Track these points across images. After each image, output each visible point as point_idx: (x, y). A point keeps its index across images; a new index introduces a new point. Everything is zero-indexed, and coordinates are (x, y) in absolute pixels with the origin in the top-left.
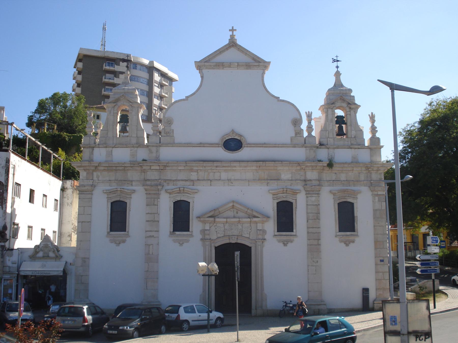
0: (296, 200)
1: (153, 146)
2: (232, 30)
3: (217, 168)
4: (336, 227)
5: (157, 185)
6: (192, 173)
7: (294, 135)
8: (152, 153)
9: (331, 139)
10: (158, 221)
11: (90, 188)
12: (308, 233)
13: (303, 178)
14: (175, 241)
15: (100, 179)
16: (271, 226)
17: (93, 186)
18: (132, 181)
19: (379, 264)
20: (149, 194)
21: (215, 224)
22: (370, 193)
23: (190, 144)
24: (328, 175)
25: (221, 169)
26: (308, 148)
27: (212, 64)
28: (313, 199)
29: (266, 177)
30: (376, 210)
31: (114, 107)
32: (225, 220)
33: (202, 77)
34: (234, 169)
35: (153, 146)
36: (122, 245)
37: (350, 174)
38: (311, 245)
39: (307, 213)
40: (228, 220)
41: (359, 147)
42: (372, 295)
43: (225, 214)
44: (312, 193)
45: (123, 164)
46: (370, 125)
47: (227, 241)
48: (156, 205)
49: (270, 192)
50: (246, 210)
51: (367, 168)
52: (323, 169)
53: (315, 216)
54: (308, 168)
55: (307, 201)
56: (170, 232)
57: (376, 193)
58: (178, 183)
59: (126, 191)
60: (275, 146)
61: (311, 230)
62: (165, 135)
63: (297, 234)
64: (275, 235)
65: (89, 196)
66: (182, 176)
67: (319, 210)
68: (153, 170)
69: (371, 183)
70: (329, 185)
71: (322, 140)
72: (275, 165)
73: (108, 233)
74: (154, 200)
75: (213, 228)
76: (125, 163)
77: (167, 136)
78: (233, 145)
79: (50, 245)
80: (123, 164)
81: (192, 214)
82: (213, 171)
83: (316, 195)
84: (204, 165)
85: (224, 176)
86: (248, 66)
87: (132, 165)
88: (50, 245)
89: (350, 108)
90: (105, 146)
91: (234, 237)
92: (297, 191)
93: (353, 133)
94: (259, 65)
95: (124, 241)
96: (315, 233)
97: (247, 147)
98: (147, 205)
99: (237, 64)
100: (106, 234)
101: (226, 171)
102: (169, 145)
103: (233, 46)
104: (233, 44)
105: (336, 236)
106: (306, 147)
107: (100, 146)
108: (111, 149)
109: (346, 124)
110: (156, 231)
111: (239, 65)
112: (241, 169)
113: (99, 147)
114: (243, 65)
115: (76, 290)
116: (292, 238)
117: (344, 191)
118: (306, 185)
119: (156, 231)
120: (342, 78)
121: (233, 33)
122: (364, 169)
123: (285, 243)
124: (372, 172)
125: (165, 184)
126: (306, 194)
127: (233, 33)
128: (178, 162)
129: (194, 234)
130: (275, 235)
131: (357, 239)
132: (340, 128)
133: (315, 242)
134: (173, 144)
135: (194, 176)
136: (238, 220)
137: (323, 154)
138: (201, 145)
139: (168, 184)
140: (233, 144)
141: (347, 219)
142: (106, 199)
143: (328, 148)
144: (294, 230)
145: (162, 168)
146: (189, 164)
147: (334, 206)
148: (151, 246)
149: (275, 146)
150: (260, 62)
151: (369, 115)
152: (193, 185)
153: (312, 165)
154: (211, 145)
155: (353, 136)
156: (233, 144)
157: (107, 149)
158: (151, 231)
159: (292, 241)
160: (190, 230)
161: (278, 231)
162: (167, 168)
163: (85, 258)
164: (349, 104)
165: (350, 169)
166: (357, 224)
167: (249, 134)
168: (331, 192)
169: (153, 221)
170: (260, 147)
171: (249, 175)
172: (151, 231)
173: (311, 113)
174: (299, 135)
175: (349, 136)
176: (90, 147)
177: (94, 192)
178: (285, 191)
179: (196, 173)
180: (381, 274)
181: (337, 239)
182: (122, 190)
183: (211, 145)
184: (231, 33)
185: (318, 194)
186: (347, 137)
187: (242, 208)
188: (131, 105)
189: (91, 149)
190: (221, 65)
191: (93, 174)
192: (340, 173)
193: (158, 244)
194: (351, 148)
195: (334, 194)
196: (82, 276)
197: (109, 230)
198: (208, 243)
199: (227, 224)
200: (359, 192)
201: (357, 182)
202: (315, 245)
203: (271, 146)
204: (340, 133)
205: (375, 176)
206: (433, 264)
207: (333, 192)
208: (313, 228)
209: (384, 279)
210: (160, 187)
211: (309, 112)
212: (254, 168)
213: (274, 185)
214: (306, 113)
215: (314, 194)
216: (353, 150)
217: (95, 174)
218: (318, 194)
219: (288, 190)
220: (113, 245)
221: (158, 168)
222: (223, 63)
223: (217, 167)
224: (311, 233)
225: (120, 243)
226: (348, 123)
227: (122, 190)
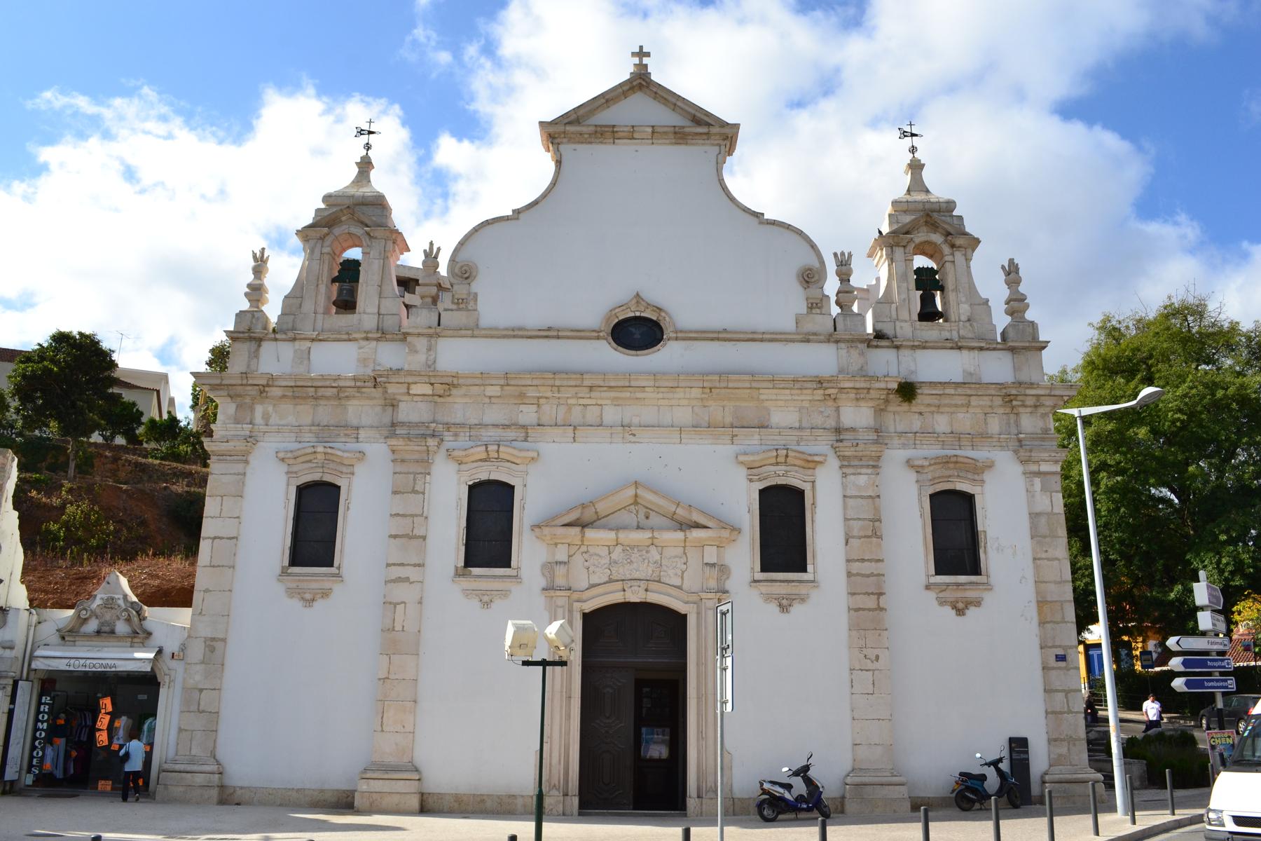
0: (813, 482)
1: (419, 335)
2: (641, 54)
3: (593, 394)
4: (927, 562)
5: (424, 436)
6: (522, 407)
7: (804, 311)
8: (416, 352)
9: (903, 324)
10: (424, 538)
11: (240, 446)
12: (849, 574)
13: (831, 423)
14: (467, 593)
15: (271, 421)
16: (744, 554)
17: (251, 439)
18: (358, 428)
19: (1053, 668)
20: (403, 461)
21: (584, 549)
22: (1019, 469)
23: (520, 329)
24: (902, 418)
25: (604, 395)
26: (842, 345)
27: (584, 129)
28: (862, 480)
29: (728, 420)
30: (1038, 514)
31: (322, 238)
32: (612, 535)
33: (559, 163)
34: (639, 395)
35: (419, 335)
36: (319, 604)
37: (961, 416)
38: (857, 610)
39: (846, 519)
40: (623, 535)
41: (983, 345)
42: (1039, 760)
43: (613, 520)
44: (856, 463)
45: (335, 380)
46: (1005, 292)
47: (617, 598)
48: (416, 492)
49: (741, 458)
50: (673, 508)
51: (1009, 399)
52: (887, 401)
53: (868, 529)
54: (844, 396)
55: (844, 486)
56: (456, 568)
57: (1034, 468)
58: (483, 432)
59: (340, 453)
60: (754, 337)
61: (856, 567)
62: (454, 307)
63: (819, 578)
64: (755, 581)
65: (239, 467)
66: (495, 414)
67: (877, 510)
68: (415, 398)
69: (1020, 441)
70: (904, 446)
71: (879, 327)
72: (754, 385)
73: (284, 572)
74: (415, 480)
75: (578, 559)
76: (338, 378)
77: (459, 309)
78: (637, 336)
79: (121, 602)
80: (335, 380)
81: (521, 519)
82: (582, 401)
83: (869, 471)
84: (558, 383)
85: (611, 414)
86: (679, 136)
87: (358, 384)
88: (121, 602)
89: (953, 246)
90: (291, 335)
91: (638, 583)
92: (817, 458)
93: (964, 310)
94: (708, 134)
95: (326, 594)
96: (868, 576)
97: (677, 339)
98: (395, 493)
99: (650, 130)
100: (278, 571)
101: (617, 402)
102: (463, 332)
103: (640, 87)
104: (641, 82)
105: (928, 587)
106: (837, 342)
107: (278, 336)
108: (308, 344)
109: (942, 289)
110: (415, 565)
111: (656, 134)
112: (660, 395)
113: (276, 340)
114: (665, 133)
115: (180, 730)
116: (803, 590)
117: (946, 462)
118: (841, 441)
119: (415, 565)
120: (927, 175)
121: (641, 60)
122: (998, 401)
123: (784, 602)
124: (1021, 410)
125: (448, 437)
126: (841, 467)
127: (641, 60)
128: (483, 378)
129: (524, 573)
130: (755, 581)
131: (988, 598)
132: (927, 300)
133: (870, 602)
134: (474, 331)
135: (527, 414)
136: (648, 534)
137: (888, 365)
138: (550, 333)
139: (456, 435)
140: (637, 333)
141: (956, 539)
142: (284, 478)
143: (897, 347)
144: (810, 568)
145: (441, 392)
146: (513, 383)
147: (920, 501)
148: (400, 608)
149: (754, 337)
150: (709, 125)
151: (1003, 267)
152: (526, 440)
153: (858, 385)
154: (578, 334)
155: (963, 318)
156: (637, 332)
157: (297, 343)
158: (402, 565)
159: (803, 599)
160: (513, 563)
161: (764, 569)
162: (454, 391)
163: (213, 639)
164: (948, 234)
165: (959, 400)
166: (985, 552)
167: (682, 306)
168: (909, 463)
169: (410, 534)
170: (712, 339)
171: (683, 415)
172: (402, 565)
173: (850, 255)
174: (818, 311)
175: (953, 317)
176: (251, 339)
177: (251, 458)
178: (783, 457)
179: (534, 408)
180: (1061, 696)
181: (932, 595)
182: (329, 451)
183: (578, 334)
184: (636, 60)
185: (874, 467)
186: (946, 321)
187: (662, 502)
188: (368, 234)
189: (254, 345)
190: (607, 134)
191: (252, 409)
192: (932, 413)
193: (420, 603)
194: (960, 348)
195: (918, 470)
196: (201, 690)
197: (286, 563)
198: (562, 601)
199: (619, 548)
200: (990, 466)
201: (980, 437)
202: (869, 610)
203: (742, 336)
204: (928, 314)
205: (1029, 423)
206: (1215, 664)
207: (917, 463)
208: (863, 560)
209: (1070, 712)
210: (432, 442)
211: (843, 254)
212: (696, 393)
213: (752, 440)
214: (835, 254)
215: (862, 466)
216: (965, 352)
217: (259, 410)
218: (874, 467)
219: (791, 454)
220: (296, 604)
221: (427, 390)
222: (614, 126)
223: (591, 388)
224: (858, 574)
225: (313, 600)
226: (950, 284)
227: (329, 451)
